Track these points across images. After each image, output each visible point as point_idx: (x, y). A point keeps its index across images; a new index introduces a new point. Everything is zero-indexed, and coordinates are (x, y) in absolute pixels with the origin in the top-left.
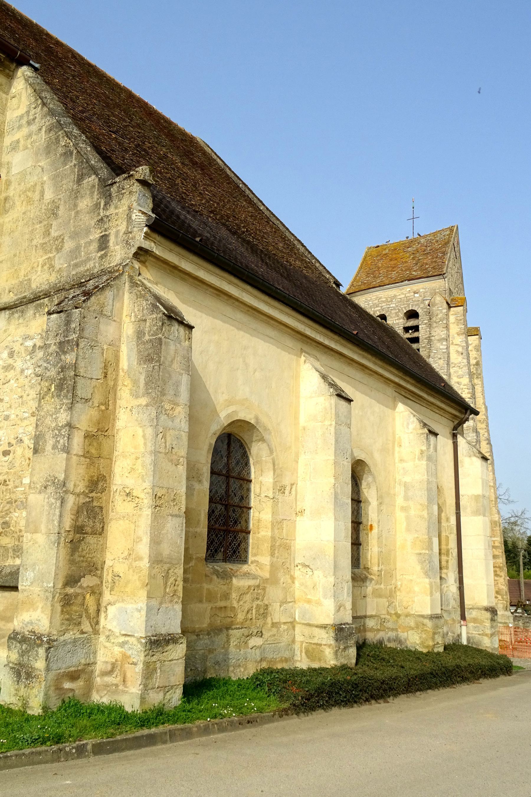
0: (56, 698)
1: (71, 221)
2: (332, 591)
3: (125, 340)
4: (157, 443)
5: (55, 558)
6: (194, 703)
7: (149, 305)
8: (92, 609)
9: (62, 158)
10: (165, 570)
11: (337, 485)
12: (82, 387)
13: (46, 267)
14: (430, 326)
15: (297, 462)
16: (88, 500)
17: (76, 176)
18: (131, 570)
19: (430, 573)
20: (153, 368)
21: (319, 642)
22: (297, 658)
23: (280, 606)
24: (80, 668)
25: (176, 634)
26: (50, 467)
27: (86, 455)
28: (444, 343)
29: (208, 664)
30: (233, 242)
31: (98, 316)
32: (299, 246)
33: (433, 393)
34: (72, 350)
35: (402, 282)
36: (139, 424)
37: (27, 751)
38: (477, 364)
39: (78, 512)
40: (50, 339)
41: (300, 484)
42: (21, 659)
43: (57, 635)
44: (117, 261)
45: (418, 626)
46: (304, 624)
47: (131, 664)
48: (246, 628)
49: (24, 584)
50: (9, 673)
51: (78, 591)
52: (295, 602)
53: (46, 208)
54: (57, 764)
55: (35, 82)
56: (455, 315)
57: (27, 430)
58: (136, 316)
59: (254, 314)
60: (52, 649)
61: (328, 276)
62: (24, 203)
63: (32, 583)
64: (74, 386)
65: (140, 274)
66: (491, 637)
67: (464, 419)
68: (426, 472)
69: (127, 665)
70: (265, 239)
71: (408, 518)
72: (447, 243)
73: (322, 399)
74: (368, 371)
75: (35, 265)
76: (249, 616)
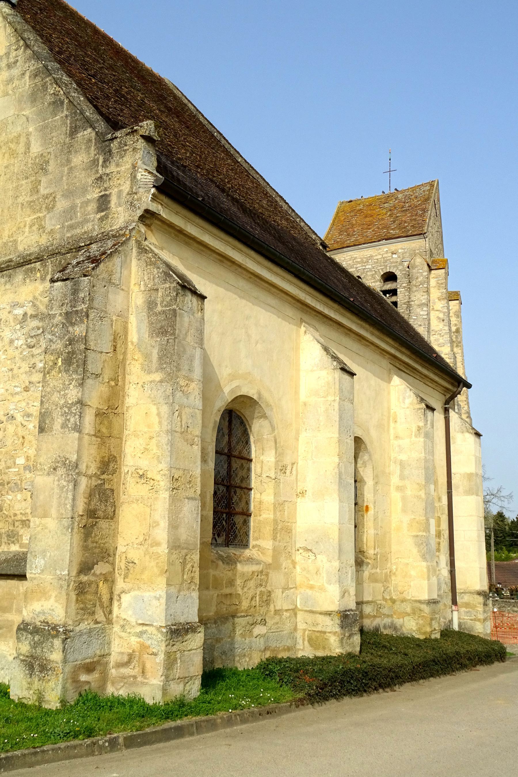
0: (73, 691)
1: (64, 178)
2: (337, 577)
3: (134, 310)
4: (173, 421)
5: (69, 544)
6: (212, 693)
7: (161, 274)
8: (105, 598)
9: (51, 107)
10: (182, 556)
11: (341, 464)
12: (92, 362)
13: (35, 228)
14: (409, 290)
15: (298, 440)
16: (99, 482)
17: (68, 128)
18: (147, 557)
19: (427, 556)
20: (168, 342)
21: (324, 629)
22: (300, 646)
23: (283, 593)
24: (95, 660)
25: (194, 623)
26: (60, 448)
27: (98, 434)
28: (425, 309)
29: (216, 654)
30: (225, 202)
31: (107, 285)
32: (281, 203)
33: (427, 365)
34: (82, 321)
35: (379, 241)
36: (152, 401)
37: (63, 745)
38: (457, 331)
39: (90, 496)
40: (54, 309)
41: (300, 463)
42: (34, 651)
43: (73, 625)
44: (120, 224)
45: (416, 612)
46: (306, 611)
47: (151, 654)
48: (250, 615)
49: (33, 572)
50: (19, 666)
51: (92, 578)
52: (296, 588)
53: (33, 162)
54: (92, 757)
55: (15, 20)
56: (436, 278)
57: (20, 406)
58: (146, 285)
59: (256, 281)
60: (69, 640)
61: (314, 237)
62: (6, 155)
63: (42, 571)
64: (85, 361)
65: (146, 239)
66: (484, 622)
67: (457, 393)
68: (423, 450)
69: (146, 656)
70: (249, 195)
71: (404, 499)
72: (427, 200)
73: (324, 373)
74: (365, 342)
75: (22, 225)
76: (253, 603)
